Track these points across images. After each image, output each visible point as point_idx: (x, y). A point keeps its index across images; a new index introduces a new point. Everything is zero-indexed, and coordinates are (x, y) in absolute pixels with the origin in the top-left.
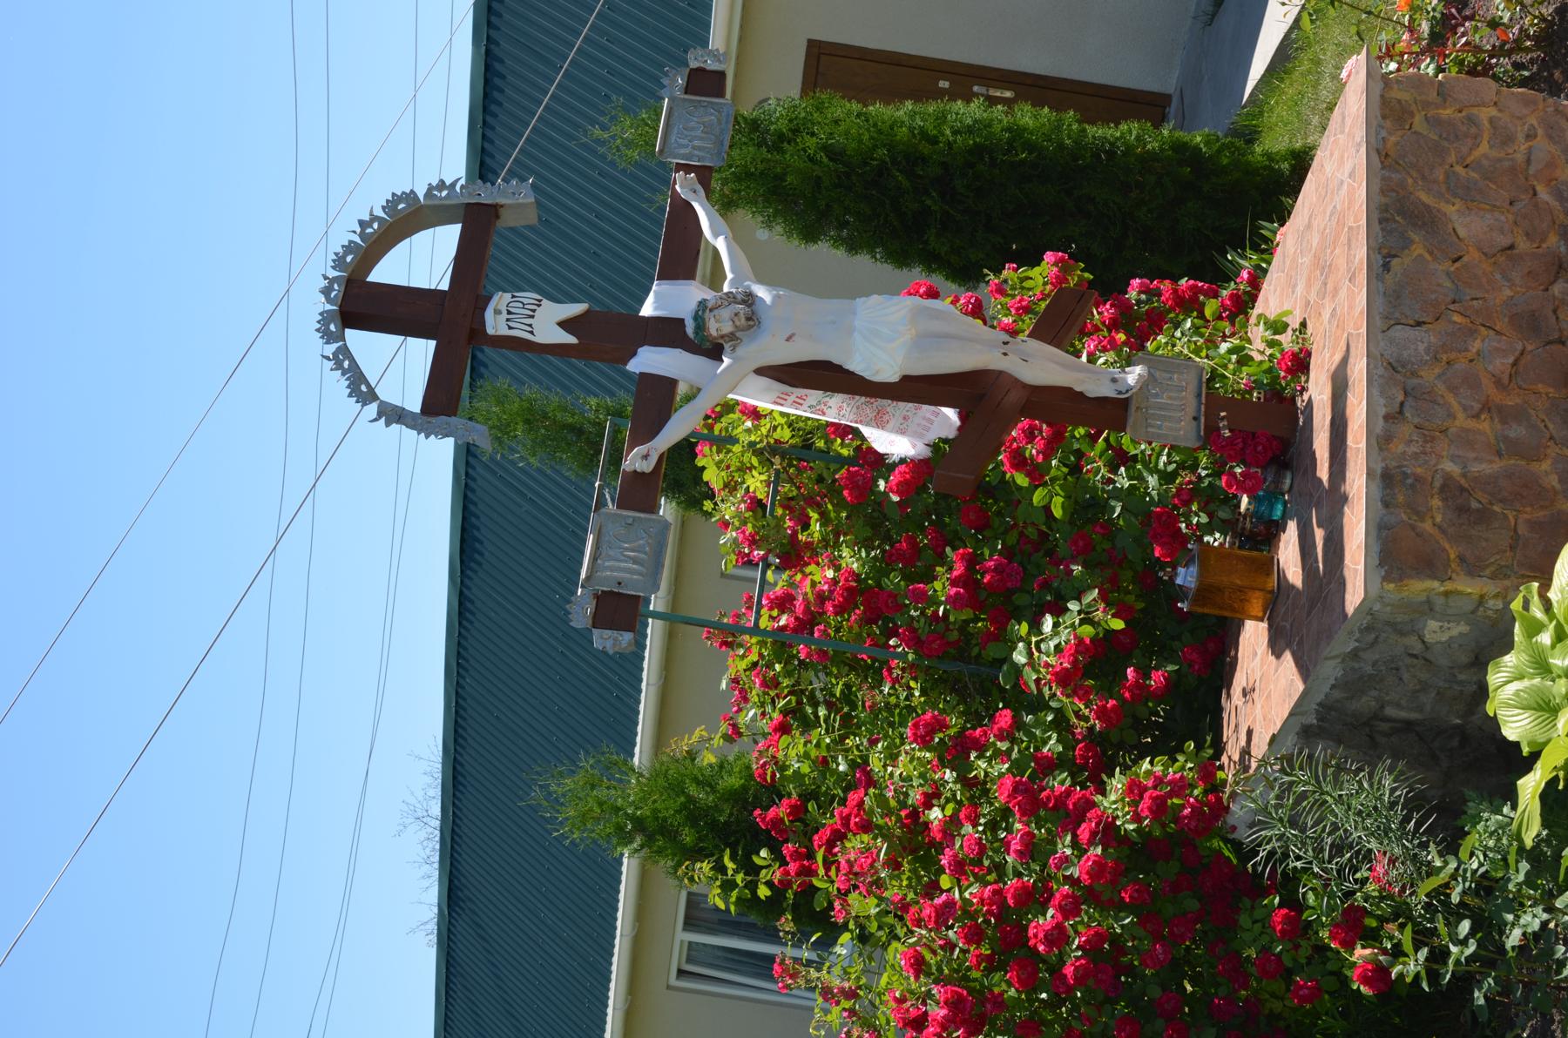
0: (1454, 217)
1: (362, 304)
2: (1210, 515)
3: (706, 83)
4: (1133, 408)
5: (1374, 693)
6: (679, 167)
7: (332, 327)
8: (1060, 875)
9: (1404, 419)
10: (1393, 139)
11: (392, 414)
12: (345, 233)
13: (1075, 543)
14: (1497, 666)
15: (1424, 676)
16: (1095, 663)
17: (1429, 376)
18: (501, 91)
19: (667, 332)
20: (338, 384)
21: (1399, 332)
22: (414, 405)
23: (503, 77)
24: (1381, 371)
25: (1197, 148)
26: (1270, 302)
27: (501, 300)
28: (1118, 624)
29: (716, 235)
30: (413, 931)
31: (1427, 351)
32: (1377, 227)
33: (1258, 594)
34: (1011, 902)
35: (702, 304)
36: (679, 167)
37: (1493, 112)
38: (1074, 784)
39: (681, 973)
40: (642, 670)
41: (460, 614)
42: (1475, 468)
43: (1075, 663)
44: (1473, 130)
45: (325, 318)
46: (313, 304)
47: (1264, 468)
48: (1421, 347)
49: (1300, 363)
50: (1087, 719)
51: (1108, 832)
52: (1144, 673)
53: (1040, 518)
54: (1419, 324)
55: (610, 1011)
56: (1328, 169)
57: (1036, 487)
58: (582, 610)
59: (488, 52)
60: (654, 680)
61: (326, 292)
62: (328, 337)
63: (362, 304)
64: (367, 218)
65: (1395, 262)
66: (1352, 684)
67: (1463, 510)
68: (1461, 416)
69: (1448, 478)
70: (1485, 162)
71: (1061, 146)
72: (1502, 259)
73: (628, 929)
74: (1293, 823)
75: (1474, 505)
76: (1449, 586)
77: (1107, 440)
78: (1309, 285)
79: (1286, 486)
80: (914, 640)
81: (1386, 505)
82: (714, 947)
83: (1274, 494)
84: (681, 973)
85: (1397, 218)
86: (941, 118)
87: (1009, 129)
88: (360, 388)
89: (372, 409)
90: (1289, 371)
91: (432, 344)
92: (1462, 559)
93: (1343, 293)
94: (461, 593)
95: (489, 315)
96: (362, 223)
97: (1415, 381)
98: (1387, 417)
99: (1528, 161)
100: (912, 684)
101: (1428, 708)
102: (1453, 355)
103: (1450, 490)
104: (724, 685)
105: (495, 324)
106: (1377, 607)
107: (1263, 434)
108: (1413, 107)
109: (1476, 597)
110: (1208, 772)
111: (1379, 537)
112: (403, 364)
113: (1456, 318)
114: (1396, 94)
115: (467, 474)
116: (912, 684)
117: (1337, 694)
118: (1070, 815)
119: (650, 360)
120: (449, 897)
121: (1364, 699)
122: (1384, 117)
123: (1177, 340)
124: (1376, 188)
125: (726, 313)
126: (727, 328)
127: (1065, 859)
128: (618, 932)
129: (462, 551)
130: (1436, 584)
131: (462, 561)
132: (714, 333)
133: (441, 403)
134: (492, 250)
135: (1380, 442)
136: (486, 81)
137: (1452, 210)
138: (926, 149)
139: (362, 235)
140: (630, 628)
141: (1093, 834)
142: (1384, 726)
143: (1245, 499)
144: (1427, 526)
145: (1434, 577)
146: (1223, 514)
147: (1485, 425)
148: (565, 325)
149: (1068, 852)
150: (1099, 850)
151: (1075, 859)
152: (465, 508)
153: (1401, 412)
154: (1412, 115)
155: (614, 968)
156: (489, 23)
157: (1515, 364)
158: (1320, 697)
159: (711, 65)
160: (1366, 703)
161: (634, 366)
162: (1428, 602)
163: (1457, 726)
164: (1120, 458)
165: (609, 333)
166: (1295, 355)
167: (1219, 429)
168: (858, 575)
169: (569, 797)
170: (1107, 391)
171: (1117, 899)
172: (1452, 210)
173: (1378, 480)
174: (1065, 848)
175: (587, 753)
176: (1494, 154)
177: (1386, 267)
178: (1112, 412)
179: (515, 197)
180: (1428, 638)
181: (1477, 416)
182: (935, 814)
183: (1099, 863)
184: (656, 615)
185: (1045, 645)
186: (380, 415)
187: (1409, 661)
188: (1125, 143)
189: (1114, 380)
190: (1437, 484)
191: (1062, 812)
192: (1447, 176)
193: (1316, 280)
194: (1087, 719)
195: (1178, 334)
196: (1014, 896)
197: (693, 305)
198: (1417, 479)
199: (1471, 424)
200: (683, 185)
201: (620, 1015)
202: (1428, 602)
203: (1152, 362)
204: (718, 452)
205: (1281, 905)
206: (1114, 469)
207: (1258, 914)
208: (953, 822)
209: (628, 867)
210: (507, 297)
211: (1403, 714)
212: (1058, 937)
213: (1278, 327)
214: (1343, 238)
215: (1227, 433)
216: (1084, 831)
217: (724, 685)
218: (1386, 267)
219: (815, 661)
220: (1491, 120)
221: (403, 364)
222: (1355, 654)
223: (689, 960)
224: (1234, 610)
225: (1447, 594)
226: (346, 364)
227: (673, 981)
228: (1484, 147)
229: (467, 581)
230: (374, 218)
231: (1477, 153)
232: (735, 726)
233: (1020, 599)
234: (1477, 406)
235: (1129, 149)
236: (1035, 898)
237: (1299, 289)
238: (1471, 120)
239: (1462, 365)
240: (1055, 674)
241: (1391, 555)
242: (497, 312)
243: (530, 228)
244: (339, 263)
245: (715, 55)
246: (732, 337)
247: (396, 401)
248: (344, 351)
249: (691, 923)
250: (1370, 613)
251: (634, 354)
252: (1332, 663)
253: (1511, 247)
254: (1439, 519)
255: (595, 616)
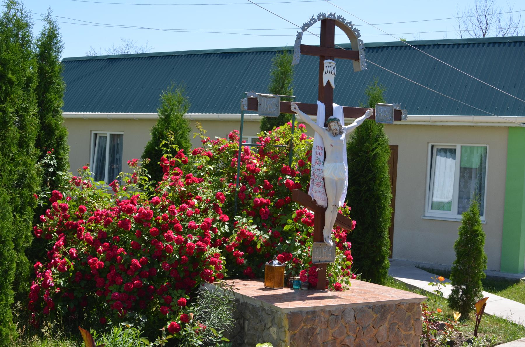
0: (385, 326)
1: (328, 24)
2: (292, 269)
3: (398, 115)
4: (321, 243)
5: (252, 317)
6: (374, 110)
7: (321, 17)
8: (187, 237)
9: (330, 316)
10: (404, 307)
11: (299, 37)
12: (348, 18)
13: (277, 233)
14: (270, 345)
15: (259, 330)
16: (247, 242)
17: (342, 322)
18: (372, 52)
19: (329, 111)
20: (306, 21)
21: (353, 312)
22: (303, 42)
23: (377, 52)
24: (342, 308)
25: (383, 262)
26: (351, 281)
27: (333, 64)
28: (259, 246)
29: (357, 122)
30: (91, 47)
31: (349, 321)
32: (380, 304)
33: (273, 285)
34: (175, 226)
35: (338, 120)
36: (374, 110)
37: (413, 335)
38: (212, 239)
39: (96, 135)
40: (195, 113)
41: (205, 54)
42: (319, 337)
43: (247, 235)
44: (408, 329)
45: (324, 15)
46: (328, 10)
47: (308, 282)
48: (349, 319)
49: (338, 288)
50: (231, 241)
51: (202, 251)
52: (242, 256)
53: (283, 222)
54: (355, 318)
55: (82, 113)
56: (392, 291)
57: (293, 220)
58: (252, 95)
59: (384, 47)
60: (192, 117)
61: (331, 14)
62: (319, 16)
63: (328, 24)
64: (352, 24)
65: (371, 310)
66: (255, 311)
67: (308, 334)
68: (332, 331)
69: (316, 329)
70: (400, 333)
71: (381, 222)
72: (375, 340)
73: (110, 116)
74: (212, 300)
75: (309, 337)
76: (287, 332)
77: (308, 239)
78: (359, 289)
79: (303, 289)
80: (243, 190)
81: (307, 313)
82: (106, 146)
83: (300, 286)
84: (96, 135)
85: (382, 309)
86: (387, 186)
87: (384, 206)
88: (306, 27)
89: (300, 30)
90: (336, 286)
91: (319, 44)
92: (295, 334)
93: (360, 297)
94: (211, 54)
95: (329, 61)
96: (351, 22)
97: (340, 318)
98: (330, 311)
99: (401, 345)
100: (229, 191)
101: (249, 332)
102: (348, 328)
103: (313, 329)
104: (216, 137)
105: (327, 63)
106: (279, 313)
107: (316, 280)
108: (412, 312)
109: (285, 339)
110: (220, 276)
111: (299, 311)
112: (313, 38)
113: (358, 328)
114: (416, 307)
115: (250, 52)
116: (229, 191)
117: (251, 307)
118: (203, 238)
119: (321, 107)
120: (112, 59)
121: (250, 315)
122: (409, 304)
123: (340, 256)
124: (390, 303)
125: (337, 127)
126: (333, 128)
127: (191, 239)
128: (108, 113)
129: (225, 53)
130: (288, 328)
131: (222, 53)
132: (331, 124)
133: (306, 50)
134: (348, 60)
135: (323, 309)
136: (375, 48)
137: (386, 325)
138: (378, 182)
139: (347, 23)
140: (248, 109)
141: (200, 246)
142: (242, 321)
143: (298, 278)
144: (302, 324)
145: (289, 328)
146: (293, 272)
147: (330, 338)
148: (328, 82)
149: (194, 239)
150: (196, 248)
151: (192, 240)
152: (239, 53)
153: (332, 315)
154: (411, 312)
155: (96, 113)
156: (393, 47)
157: (347, 345)
158: (249, 302)
159: (403, 116)
160: (248, 315)
161: (319, 103)
162: (282, 327)
163: (244, 342)
164: (303, 242)
165: (327, 95)
166: (340, 287)
167: (317, 268)
168: (258, 173)
169: (172, 95)
170: (325, 236)
171: (182, 254)
172: (386, 325)
173: (313, 310)
174: (195, 238)
175: (189, 99)
176: (402, 336)
177: (370, 308)
178: (319, 238)
179: (362, 64)
180: (271, 329)
181: (333, 336)
182: (196, 202)
183: (193, 248)
184: (242, 116)
185: (248, 226)
186: (299, 33)
187: (263, 324)
188: (383, 241)
189: (328, 237)
190: (314, 326)
191: (203, 237)
192: (396, 323)
193: (359, 292)
194: (231, 241)
195: (341, 254)
196: (177, 226)
197: (338, 118)
198: (315, 321)
199: (330, 335)
200: (369, 111)
201: (81, 117)
202: (282, 327)
203: (334, 248)
204: (289, 129)
205: (187, 300)
206: (299, 241)
207: (183, 294)
208: (192, 206)
209: (155, 115)
210: (335, 65)
211: (246, 326)
212: (169, 239)
213: (347, 283)
214: (375, 296)
215: (317, 270)
216: (200, 243)
217: (216, 137)
218: (370, 308)
219: (230, 165)
220: (411, 334)
221: (313, 38)
222: (264, 309)
223: (100, 137)
224: (267, 278)
225: (285, 331)
226: (312, 22)
227: (93, 132)
228: (404, 333)
229: (216, 55)
230: (352, 26)
231: (402, 331)
232: (206, 142)
233: (258, 219)
234: (335, 336)
235: (382, 242)
236: (177, 231)
237: (357, 287)
238: (411, 328)
239: (346, 331)
240: (243, 230)
241: (294, 314)
242: (330, 63)
243: (353, 70)
244: (339, 17)
245: (406, 117)
246: (330, 129)
247: (303, 37)
248: (315, 21)
249: (112, 136)
250: (277, 311)
251: (322, 102)
252: (261, 304)
253: (378, 342)
254: (305, 327)
255: (251, 98)
